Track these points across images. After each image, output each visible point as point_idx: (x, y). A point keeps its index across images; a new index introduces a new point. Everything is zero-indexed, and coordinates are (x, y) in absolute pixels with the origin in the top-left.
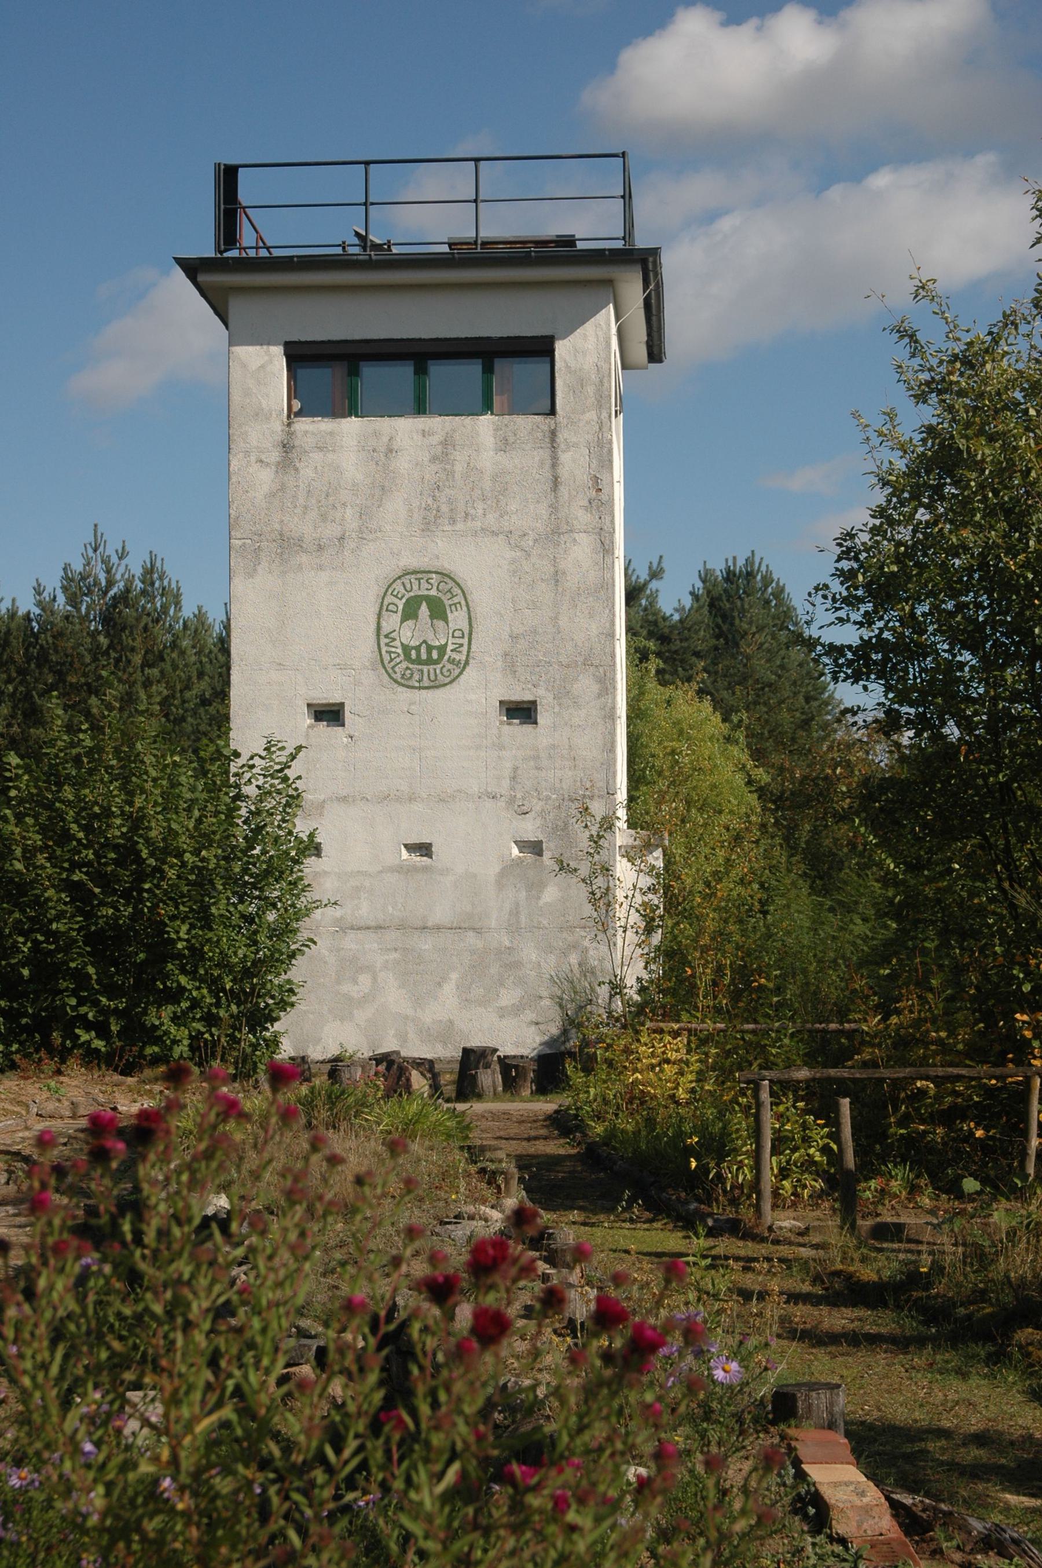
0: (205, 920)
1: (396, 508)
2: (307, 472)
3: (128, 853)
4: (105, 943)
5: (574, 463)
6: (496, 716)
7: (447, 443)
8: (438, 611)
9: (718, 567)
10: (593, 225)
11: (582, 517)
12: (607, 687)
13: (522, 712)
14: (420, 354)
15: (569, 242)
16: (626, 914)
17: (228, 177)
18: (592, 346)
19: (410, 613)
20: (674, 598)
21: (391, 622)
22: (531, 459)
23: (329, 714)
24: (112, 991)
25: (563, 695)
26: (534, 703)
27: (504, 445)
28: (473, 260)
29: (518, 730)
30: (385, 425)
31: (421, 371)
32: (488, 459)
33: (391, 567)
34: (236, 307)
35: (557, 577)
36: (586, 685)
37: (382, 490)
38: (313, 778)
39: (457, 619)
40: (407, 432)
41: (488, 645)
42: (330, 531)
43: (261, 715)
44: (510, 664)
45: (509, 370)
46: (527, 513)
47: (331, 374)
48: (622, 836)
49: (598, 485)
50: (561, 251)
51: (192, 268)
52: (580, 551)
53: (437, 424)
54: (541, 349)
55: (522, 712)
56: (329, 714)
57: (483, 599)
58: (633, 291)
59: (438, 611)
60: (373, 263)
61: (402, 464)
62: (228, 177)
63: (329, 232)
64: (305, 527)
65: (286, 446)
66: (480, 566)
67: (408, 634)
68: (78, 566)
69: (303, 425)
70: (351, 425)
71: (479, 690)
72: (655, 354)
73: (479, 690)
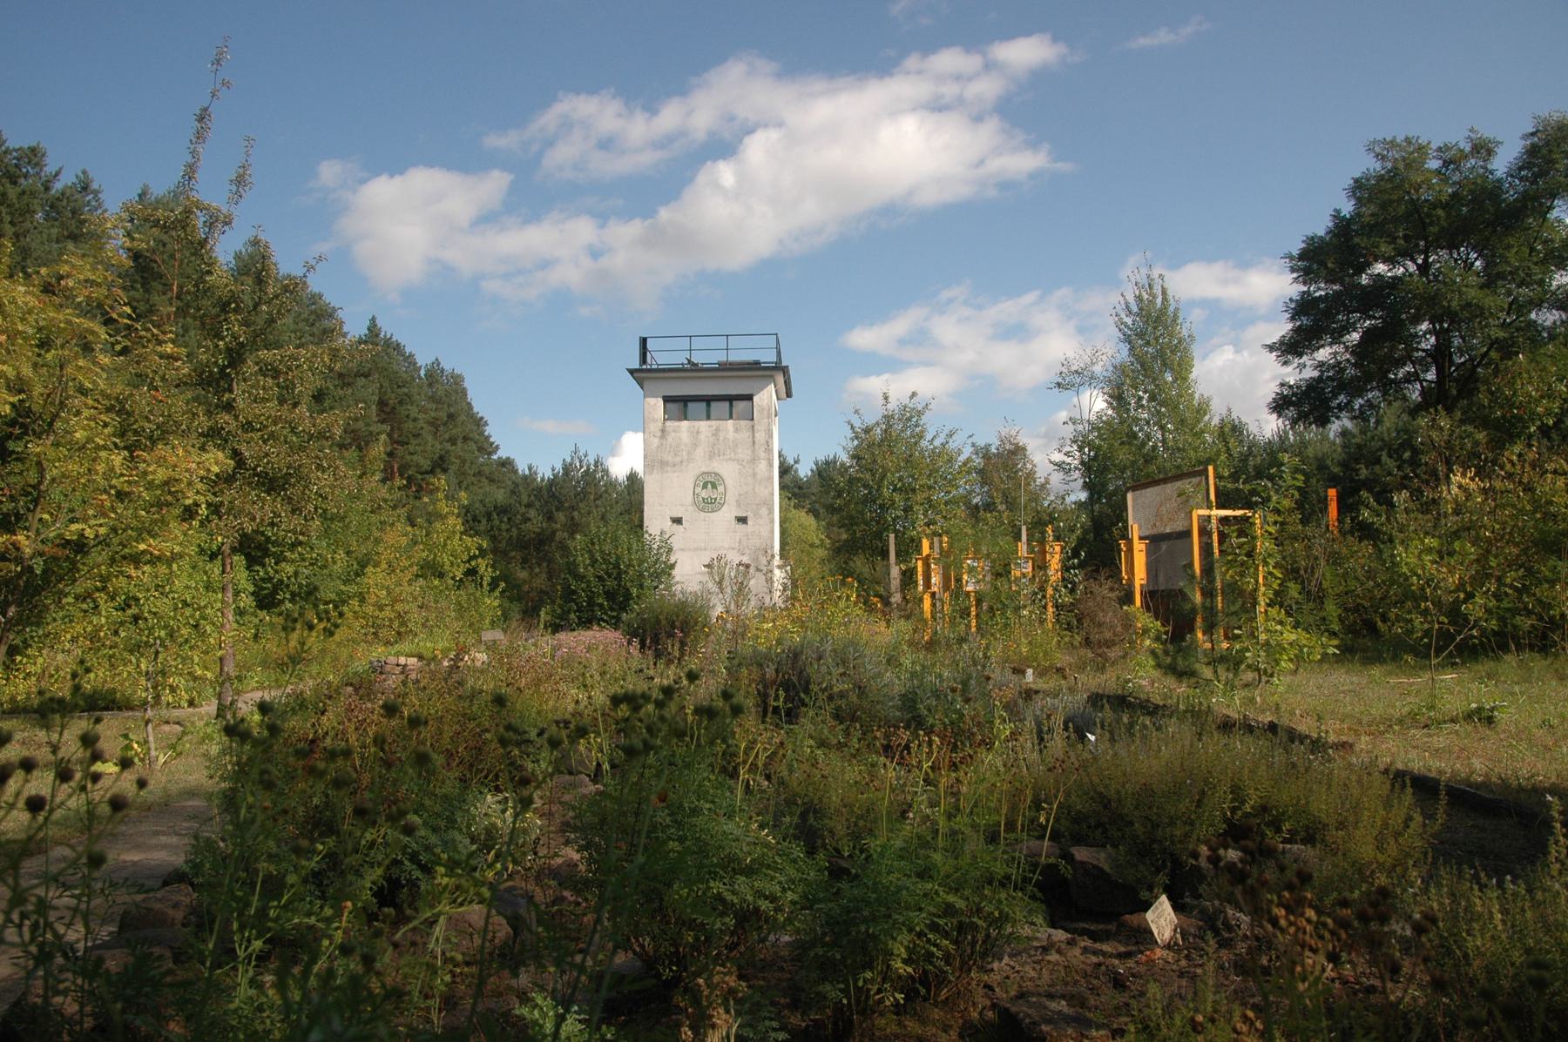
0: (641, 586)
1: (700, 452)
2: (670, 439)
3: (617, 566)
4: (610, 595)
5: (760, 436)
6: (734, 522)
7: (718, 430)
8: (714, 486)
9: (821, 458)
10: (768, 357)
11: (763, 455)
12: (771, 511)
13: (742, 520)
14: (708, 400)
15: (757, 363)
16: (777, 586)
17: (644, 341)
18: (766, 396)
19: (705, 487)
20: (804, 471)
21: (698, 490)
22: (745, 435)
23: (677, 521)
24: (612, 609)
25: (756, 514)
26: (256, 242)
27: (736, 430)
28: (726, 368)
29: (741, 526)
30: (697, 423)
31: (708, 405)
32: (731, 435)
33: (698, 472)
34: (646, 384)
35: (754, 475)
36: (764, 511)
37: (695, 446)
38: (676, 543)
39: (721, 489)
40: (703, 425)
41: (731, 497)
42: (678, 459)
43: (655, 522)
44: (739, 504)
45: (740, 406)
46: (744, 453)
47: (679, 405)
48: (777, 561)
49: (768, 444)
50: (755, 366)
51: (632, 372)
52: (762, 466)
53: (713, 423)
54: (749, 398)
55: (742, 520)
56: (677, 521)
57: (729, 482)
58: (780, 379)
59: (714, 486)
60: (693, 370)
61: (702, 437)
62: (644, 341)
63: (679, 359)
64: (669, 458)
65: (663, 431)
66: (728, 471)
67: (704, 494)
68: (568, 460)
69: (669, 423)
70: (685, 423)
71: (728, 513)
72: (789, 395)
73: (728, 513)
